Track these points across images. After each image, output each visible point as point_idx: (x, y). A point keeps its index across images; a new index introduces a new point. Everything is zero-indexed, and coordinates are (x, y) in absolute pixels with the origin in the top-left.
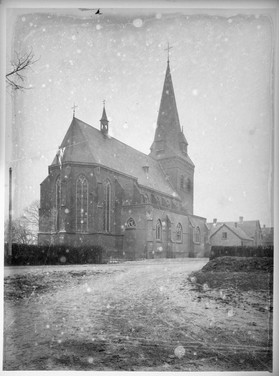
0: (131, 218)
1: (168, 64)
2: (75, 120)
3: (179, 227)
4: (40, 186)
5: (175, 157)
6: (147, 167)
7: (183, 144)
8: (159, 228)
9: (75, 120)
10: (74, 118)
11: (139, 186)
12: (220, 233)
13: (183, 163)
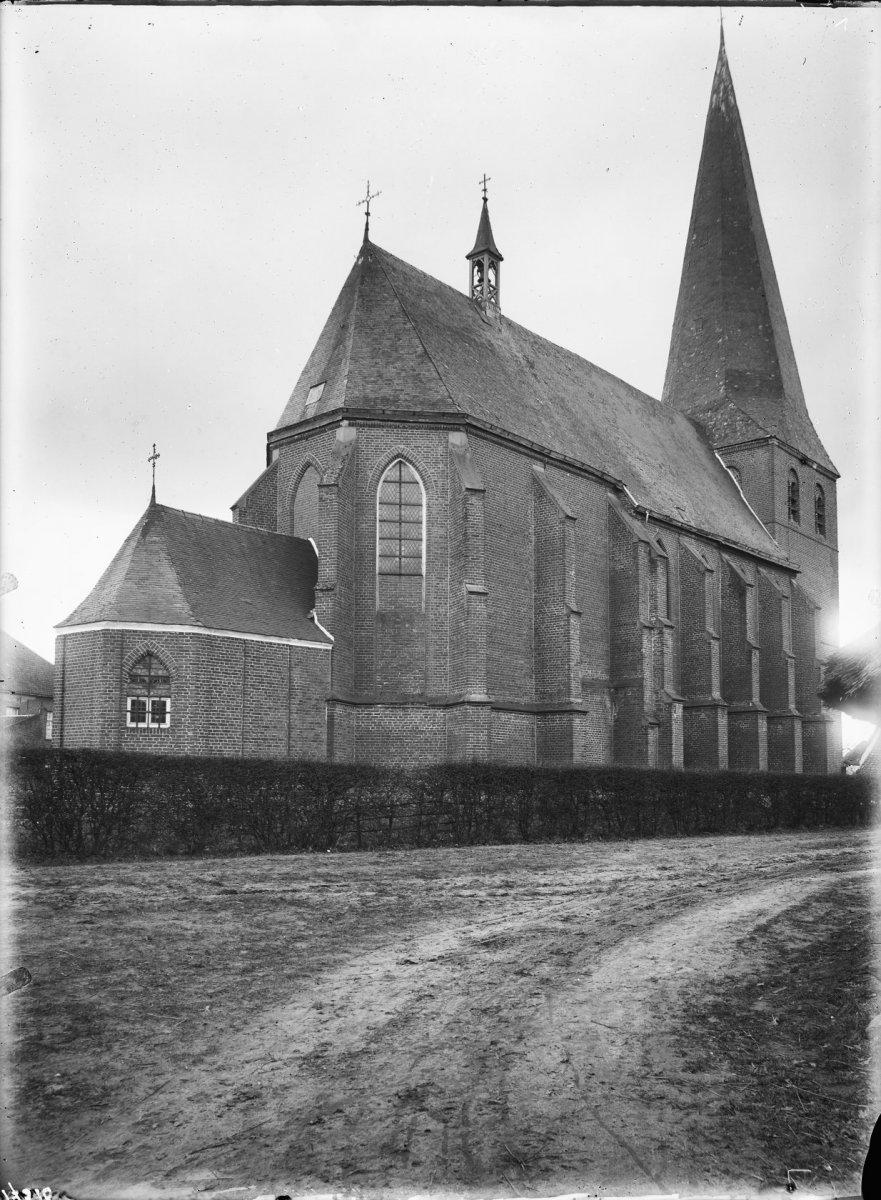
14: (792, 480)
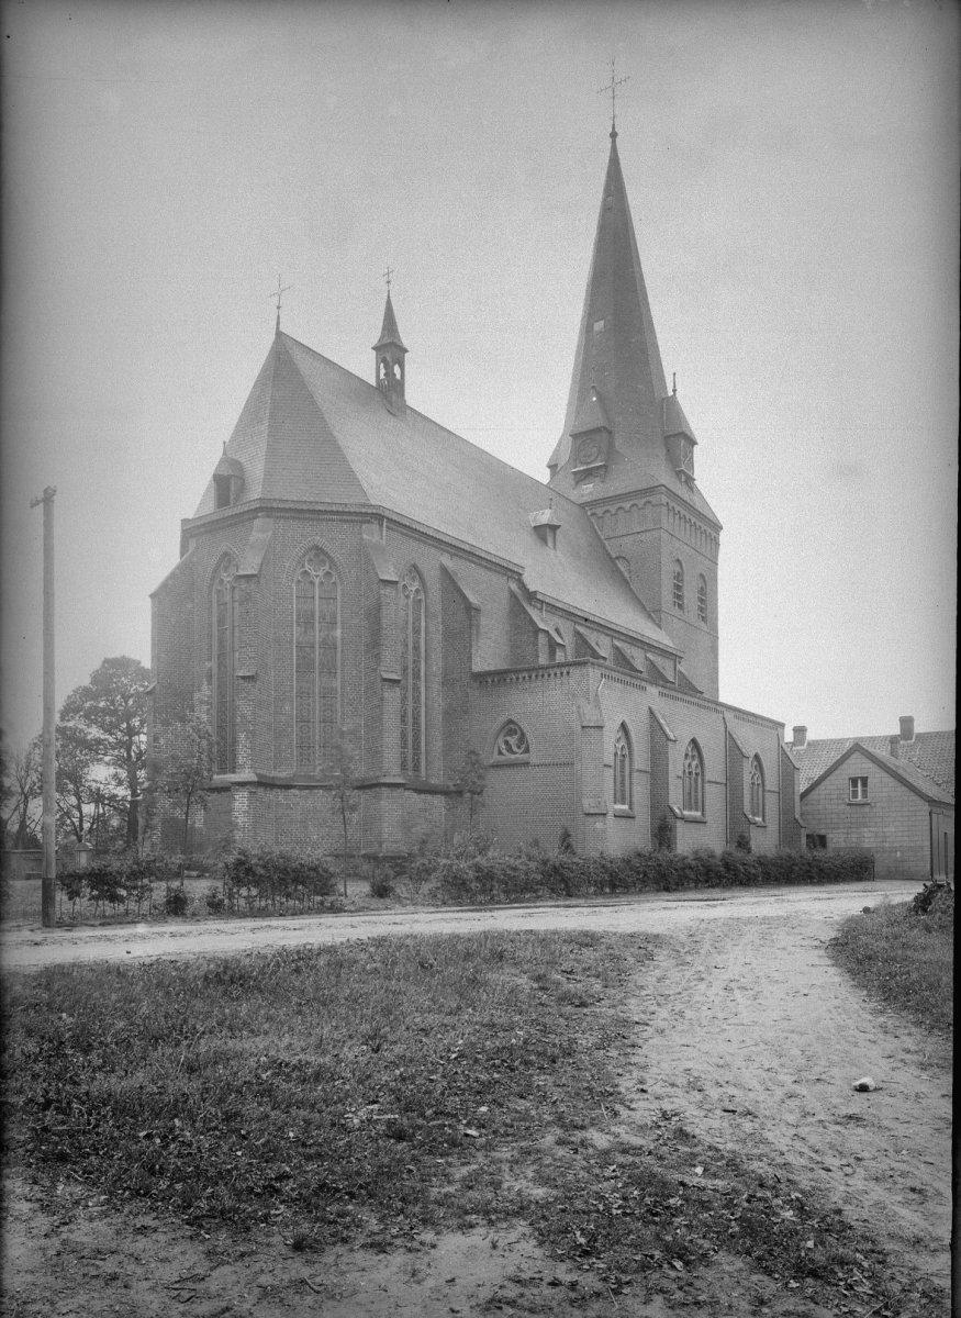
0: (511, 721)
1: (614, 142)
3: (693, 756)
4: (149, 600)
5: (651, 490)
6: (554, 528)
7: (676, 443)
8: (623, 762)
10: (279, 334)
11: (531, 596)
13: (683, 512)
14: (678, 569)
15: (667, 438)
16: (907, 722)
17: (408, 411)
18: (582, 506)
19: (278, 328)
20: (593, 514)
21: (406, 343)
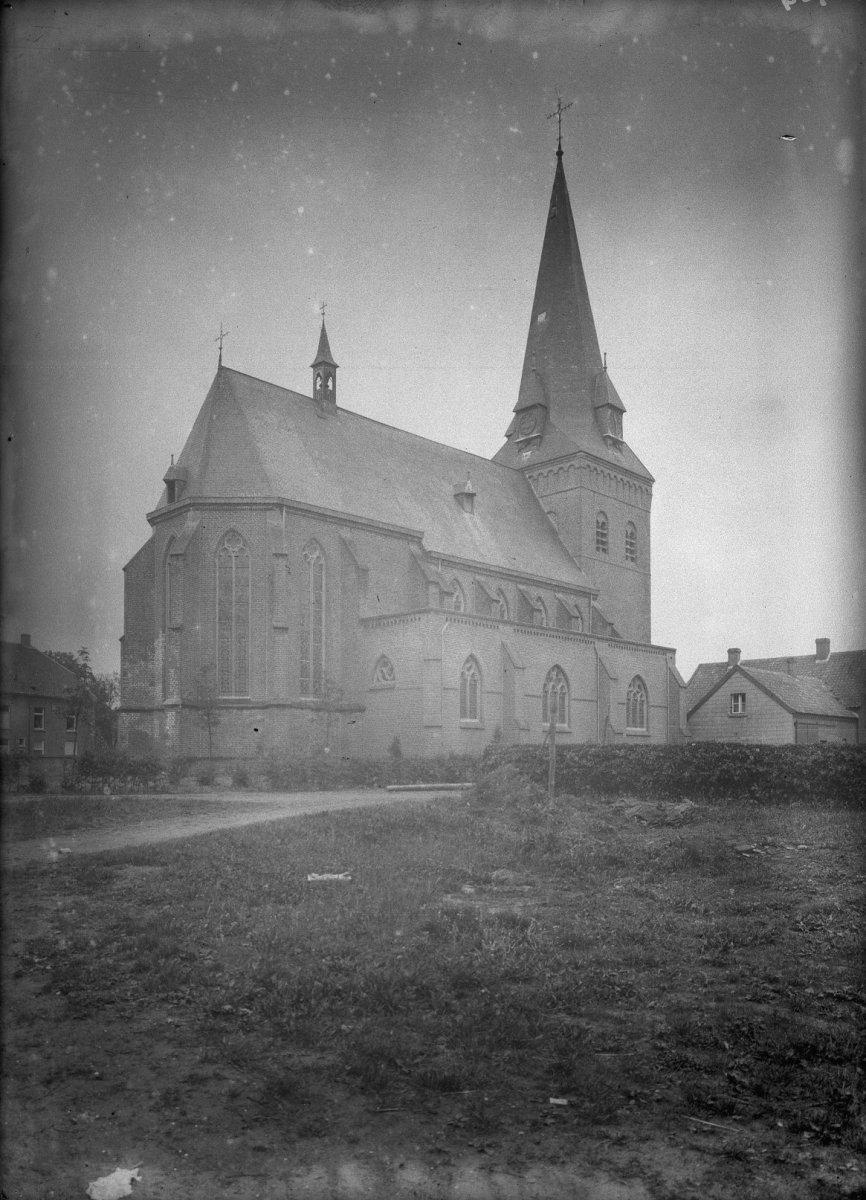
0: (383, 656)
1: (560, 159)
2: (222, 370)
6: (471, 496)
7: (607, 411)
9: (222, 370)
10: (221, 368)
12: (723, 695)
15: (596, 408)
16: (823, 644)
17: (339, 412)
18: (521, 471)
19: (220, 365)
20: (530, 477)
21: (336, 359)
